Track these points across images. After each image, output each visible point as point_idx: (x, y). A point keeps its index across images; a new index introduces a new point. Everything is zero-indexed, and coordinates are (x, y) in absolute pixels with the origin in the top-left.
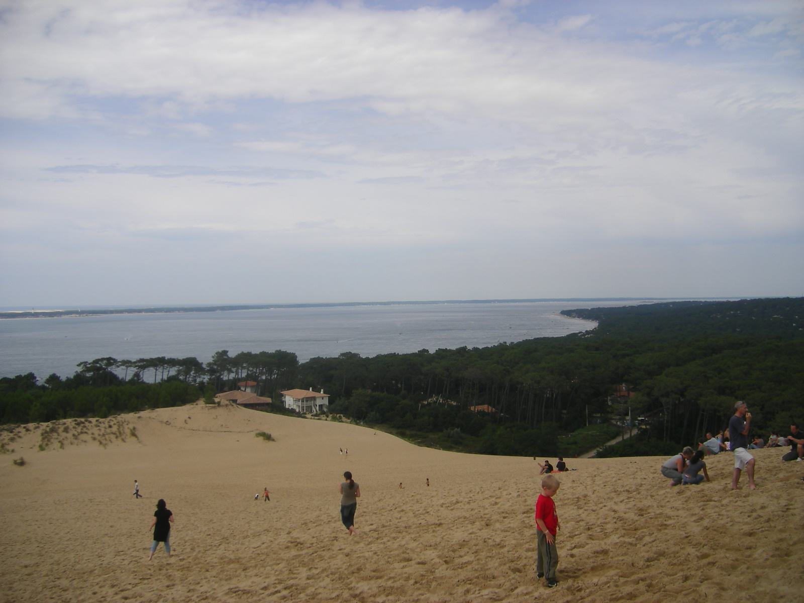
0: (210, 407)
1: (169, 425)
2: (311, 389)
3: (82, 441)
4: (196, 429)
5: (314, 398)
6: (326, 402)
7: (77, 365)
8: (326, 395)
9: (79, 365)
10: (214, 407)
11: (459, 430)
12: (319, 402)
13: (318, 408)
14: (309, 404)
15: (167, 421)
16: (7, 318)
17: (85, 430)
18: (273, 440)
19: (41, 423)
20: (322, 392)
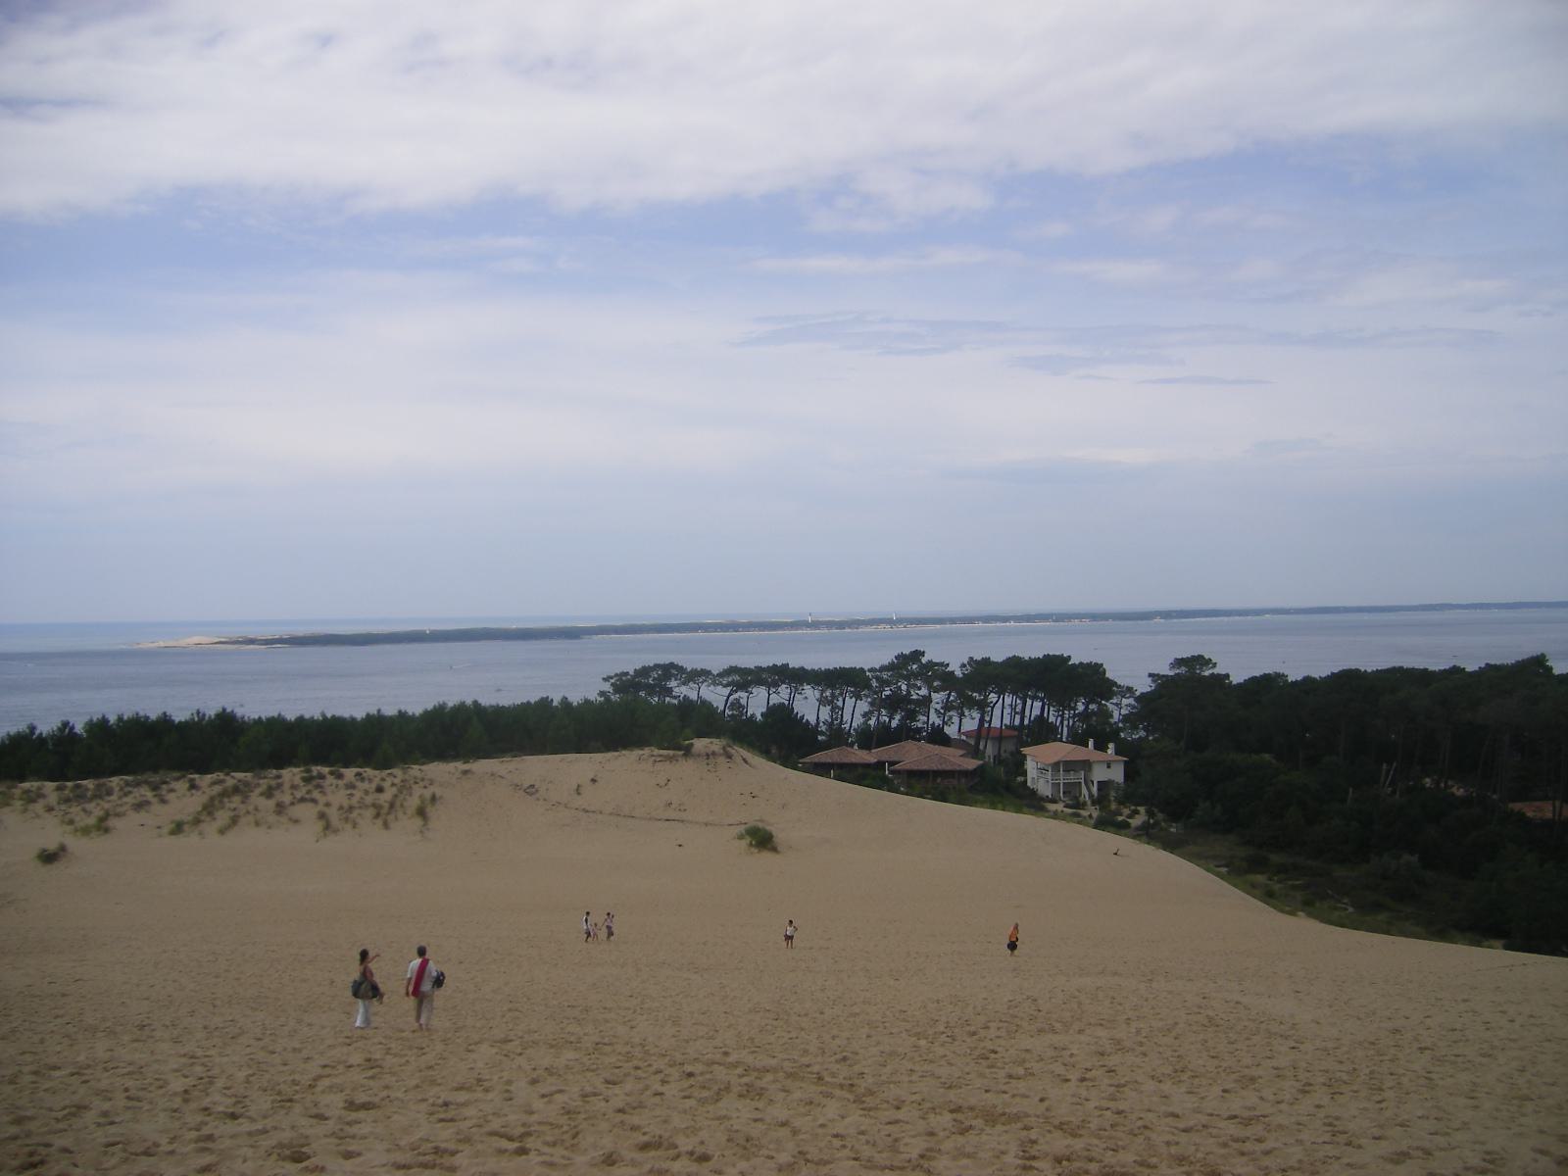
0: (661, 756)
1: (531, 794)
2: (1091, 743)
3: (290, 819)
4: (593, 809)
5: (1086, 765)
6: (1117, 774)
7: (604, 679)
8: (1120, 758)
9: (605, 680)
10: (670, 759)
11: (1414, 859)
12: (1099, 774)
13: (1095, 790)
14: (1072, 777)
15: (532, 786)
16: (775, 630)
17: (316, 794)
18: (774, 850)
19: (232, 774)
20: (1109, 751)
